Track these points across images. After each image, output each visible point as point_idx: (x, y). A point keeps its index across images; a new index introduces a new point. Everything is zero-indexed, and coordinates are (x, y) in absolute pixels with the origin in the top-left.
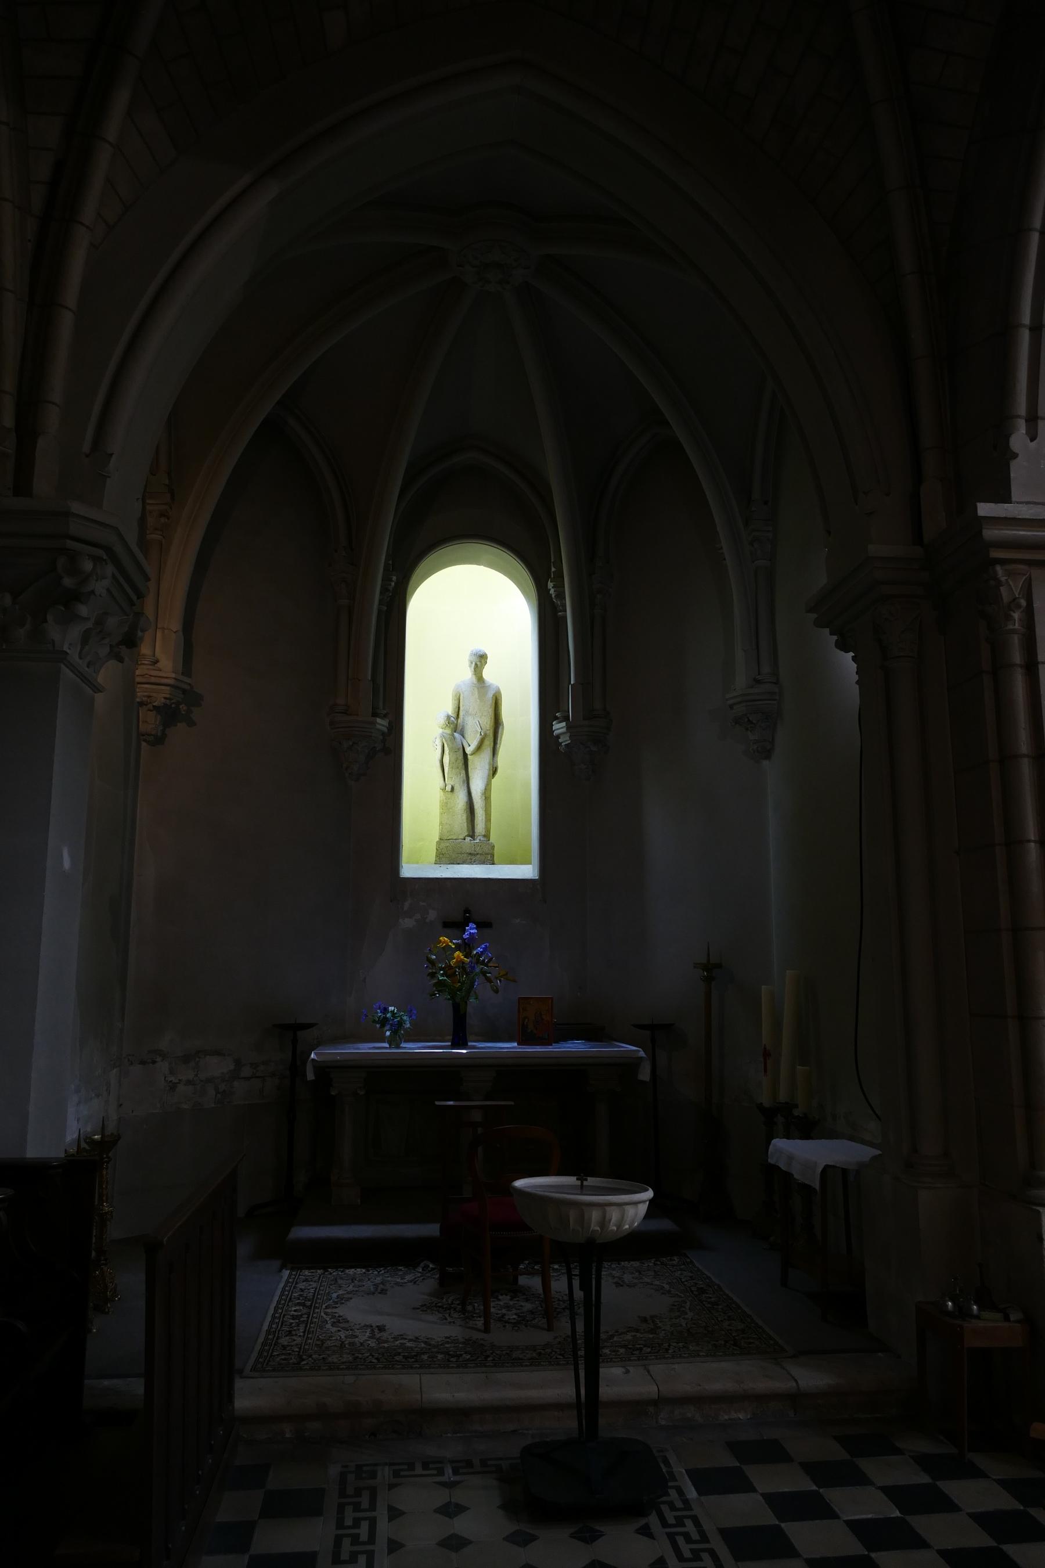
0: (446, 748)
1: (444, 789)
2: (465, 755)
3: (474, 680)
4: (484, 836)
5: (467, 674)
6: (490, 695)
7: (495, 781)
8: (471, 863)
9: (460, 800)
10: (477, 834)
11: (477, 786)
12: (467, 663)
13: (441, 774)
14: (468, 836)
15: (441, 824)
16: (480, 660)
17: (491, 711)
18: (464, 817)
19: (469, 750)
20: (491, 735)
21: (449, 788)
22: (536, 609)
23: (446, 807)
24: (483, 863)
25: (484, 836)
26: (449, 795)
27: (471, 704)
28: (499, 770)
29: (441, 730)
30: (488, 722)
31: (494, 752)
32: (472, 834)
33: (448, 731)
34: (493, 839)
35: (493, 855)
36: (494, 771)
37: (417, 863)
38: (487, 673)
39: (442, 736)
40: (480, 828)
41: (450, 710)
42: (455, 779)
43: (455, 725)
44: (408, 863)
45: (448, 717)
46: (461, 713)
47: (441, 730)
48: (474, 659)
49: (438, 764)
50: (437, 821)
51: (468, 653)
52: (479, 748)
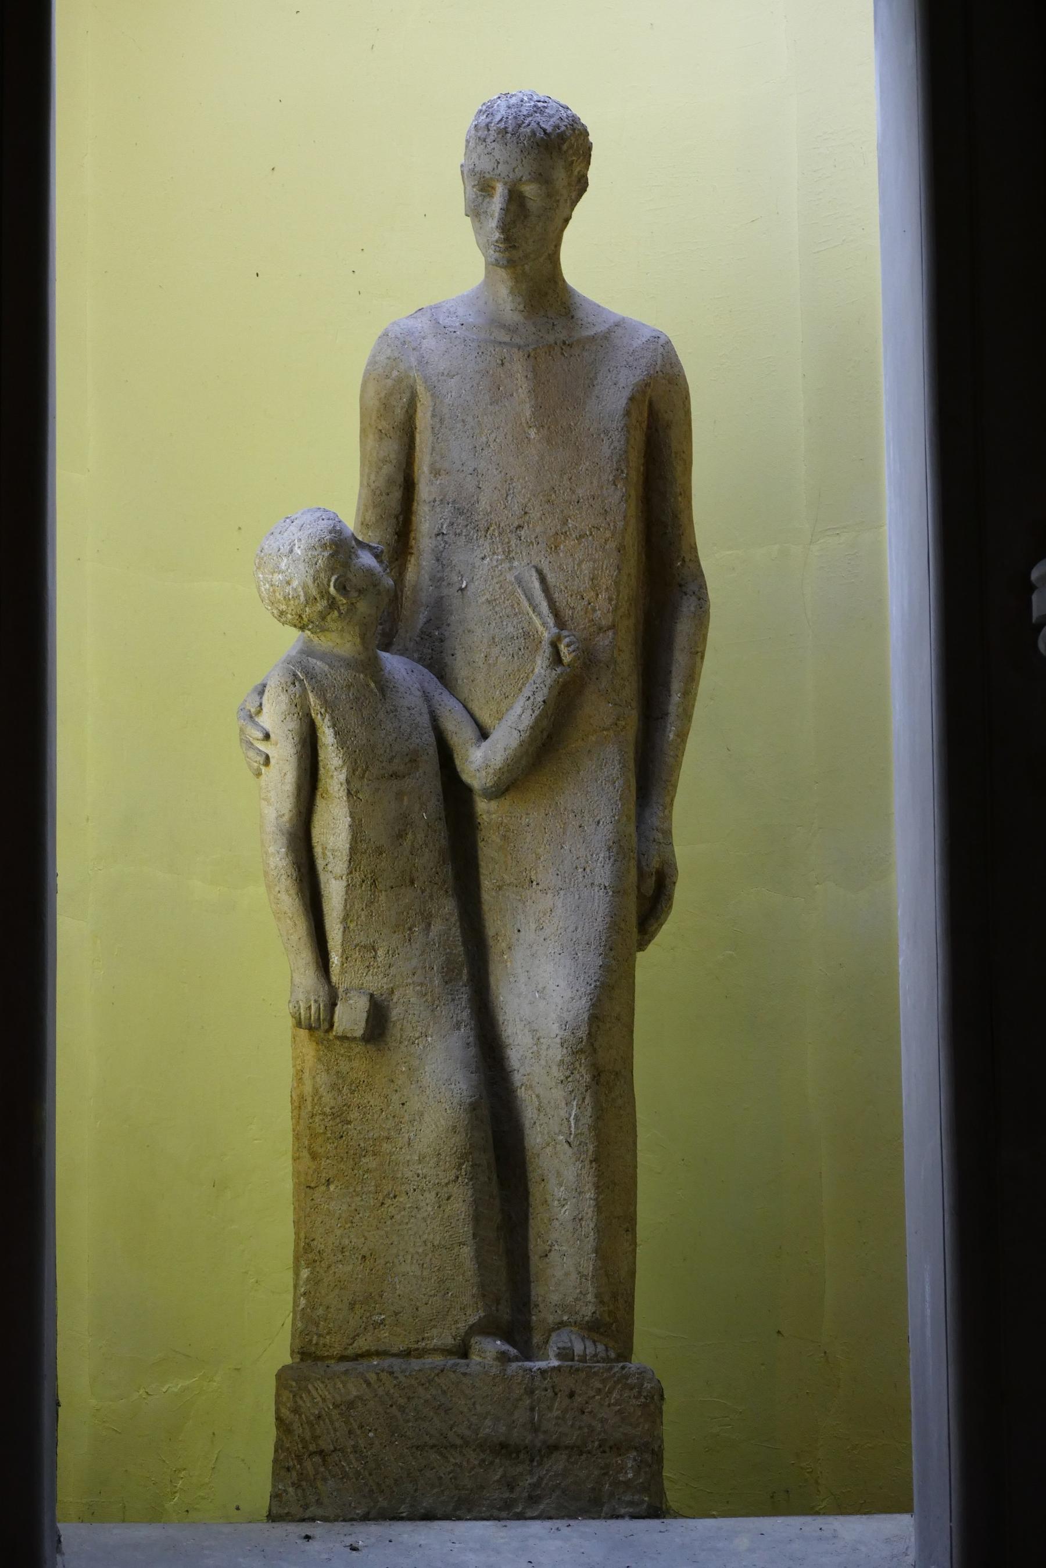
0: (327, 736)
1: (318, 1026)
2: (456, 795)
3: (506, 302)
4: (594, 1328)
5: (454, 264)
6: (613, 394)
7: (651, 964)
8: (507, 1510)
9: (434, 1079)
10: (544, 1315)
11: (541, 993)
12: (455, 192)
13: (299, 930)
14: (488, 1328)
15: (306, 1252)
16: (536, 170)
17: (619, 502)
18: (460, 1205)
19: (480, 762)
20: (627, 662)
21: (351, 1016)
22: (47, 1105)
23: (335, 1143)
24: (588, 1504)
25: (594, 1328)
26: (357, 1064)
27: (477, 458)
28: (684, 894)
29: (289, 640)
30: (595, 573)
31: (650, 773)
32: (512, 1315)
33: (340, 642)
34: (648, 1347)
35: (652, 1455)
36: (646, 896)
37: (155, 1515)
38: (590, 256)
39: (302, 676)
40: (564, 1265)
41: (341, 491)
42: (400, 968)
43: (378, 598)
44: (92, 1514)
45: (339, 548)
46: (426, 522)
47: (289, 640)
48: (503, 161)
49: (277, 858)
50: (279, 1233)
51: (464, 121)
52: (547, 748)
